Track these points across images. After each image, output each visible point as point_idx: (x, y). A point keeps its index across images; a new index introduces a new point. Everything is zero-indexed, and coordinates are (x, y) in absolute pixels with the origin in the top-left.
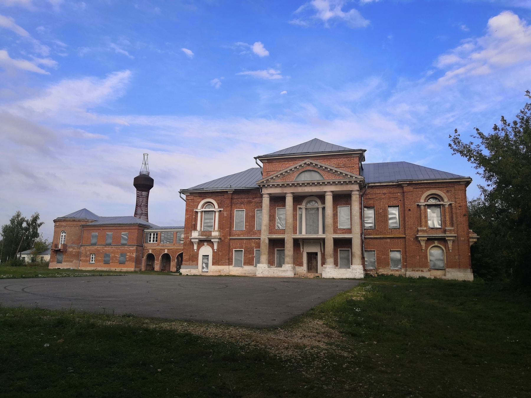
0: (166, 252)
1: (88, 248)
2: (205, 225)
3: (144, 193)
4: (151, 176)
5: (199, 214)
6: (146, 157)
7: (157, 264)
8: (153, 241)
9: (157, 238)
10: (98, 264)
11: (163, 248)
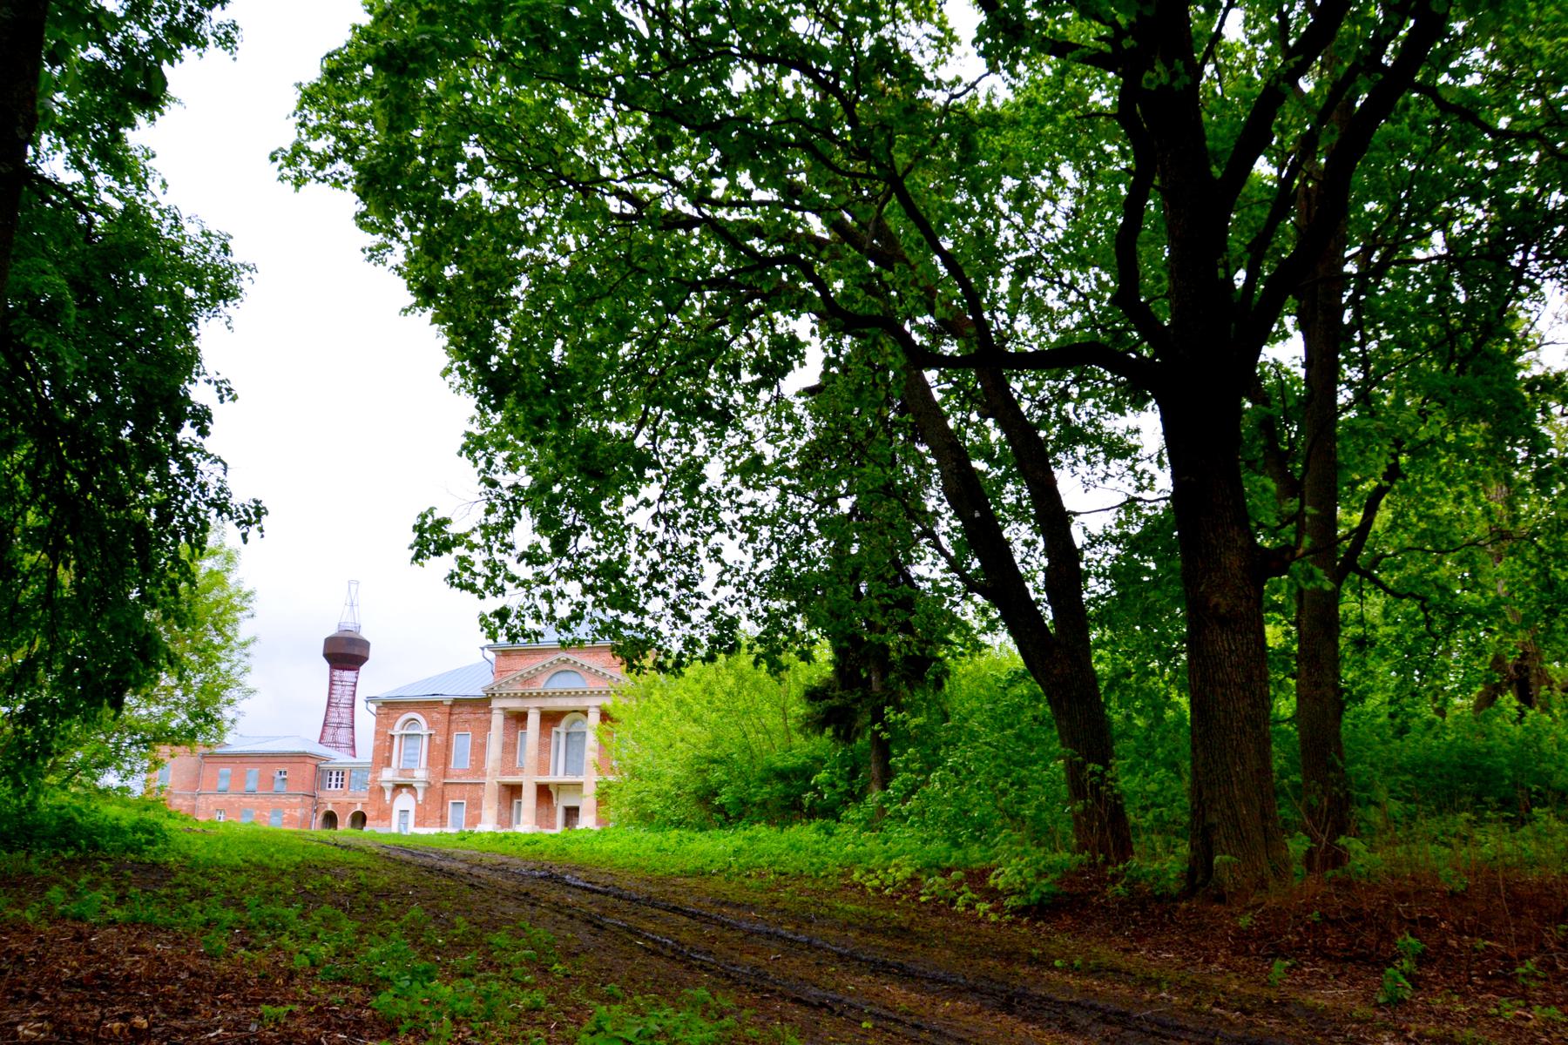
0: (359, 808)
1: (212, 798)
3: (348, 675)
5: (396, 740)
6: (353, 587)
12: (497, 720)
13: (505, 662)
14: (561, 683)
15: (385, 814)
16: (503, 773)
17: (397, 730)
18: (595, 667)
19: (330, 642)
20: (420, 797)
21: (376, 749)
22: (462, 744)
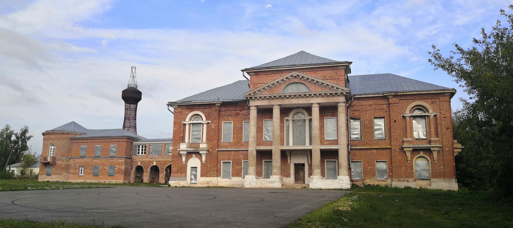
0: (155, 164)
1: (77, 160)
2: (193, 137)
3: (132, 106)
4: (139, 89)
5: (187, 127)
6: (134, 70)
7: (146, 176)
8: (142, 153)
9: (145, 150)
10: (87, 176)
11: (151, 160)
12: (253, 113)
13: (256, 79)
14: (292, 89)
15: (182, 170)
16: (257, 145)
17: (187, 121)
18: (311, 78)
19: (124, 92)
20: (204, 159)
21: (175, 133)
22: (227, 128)
